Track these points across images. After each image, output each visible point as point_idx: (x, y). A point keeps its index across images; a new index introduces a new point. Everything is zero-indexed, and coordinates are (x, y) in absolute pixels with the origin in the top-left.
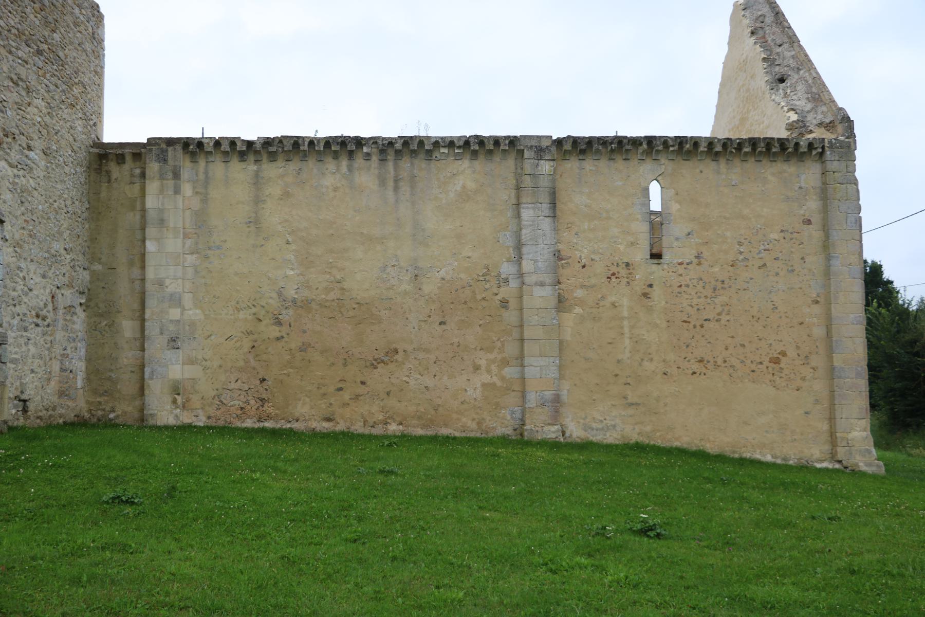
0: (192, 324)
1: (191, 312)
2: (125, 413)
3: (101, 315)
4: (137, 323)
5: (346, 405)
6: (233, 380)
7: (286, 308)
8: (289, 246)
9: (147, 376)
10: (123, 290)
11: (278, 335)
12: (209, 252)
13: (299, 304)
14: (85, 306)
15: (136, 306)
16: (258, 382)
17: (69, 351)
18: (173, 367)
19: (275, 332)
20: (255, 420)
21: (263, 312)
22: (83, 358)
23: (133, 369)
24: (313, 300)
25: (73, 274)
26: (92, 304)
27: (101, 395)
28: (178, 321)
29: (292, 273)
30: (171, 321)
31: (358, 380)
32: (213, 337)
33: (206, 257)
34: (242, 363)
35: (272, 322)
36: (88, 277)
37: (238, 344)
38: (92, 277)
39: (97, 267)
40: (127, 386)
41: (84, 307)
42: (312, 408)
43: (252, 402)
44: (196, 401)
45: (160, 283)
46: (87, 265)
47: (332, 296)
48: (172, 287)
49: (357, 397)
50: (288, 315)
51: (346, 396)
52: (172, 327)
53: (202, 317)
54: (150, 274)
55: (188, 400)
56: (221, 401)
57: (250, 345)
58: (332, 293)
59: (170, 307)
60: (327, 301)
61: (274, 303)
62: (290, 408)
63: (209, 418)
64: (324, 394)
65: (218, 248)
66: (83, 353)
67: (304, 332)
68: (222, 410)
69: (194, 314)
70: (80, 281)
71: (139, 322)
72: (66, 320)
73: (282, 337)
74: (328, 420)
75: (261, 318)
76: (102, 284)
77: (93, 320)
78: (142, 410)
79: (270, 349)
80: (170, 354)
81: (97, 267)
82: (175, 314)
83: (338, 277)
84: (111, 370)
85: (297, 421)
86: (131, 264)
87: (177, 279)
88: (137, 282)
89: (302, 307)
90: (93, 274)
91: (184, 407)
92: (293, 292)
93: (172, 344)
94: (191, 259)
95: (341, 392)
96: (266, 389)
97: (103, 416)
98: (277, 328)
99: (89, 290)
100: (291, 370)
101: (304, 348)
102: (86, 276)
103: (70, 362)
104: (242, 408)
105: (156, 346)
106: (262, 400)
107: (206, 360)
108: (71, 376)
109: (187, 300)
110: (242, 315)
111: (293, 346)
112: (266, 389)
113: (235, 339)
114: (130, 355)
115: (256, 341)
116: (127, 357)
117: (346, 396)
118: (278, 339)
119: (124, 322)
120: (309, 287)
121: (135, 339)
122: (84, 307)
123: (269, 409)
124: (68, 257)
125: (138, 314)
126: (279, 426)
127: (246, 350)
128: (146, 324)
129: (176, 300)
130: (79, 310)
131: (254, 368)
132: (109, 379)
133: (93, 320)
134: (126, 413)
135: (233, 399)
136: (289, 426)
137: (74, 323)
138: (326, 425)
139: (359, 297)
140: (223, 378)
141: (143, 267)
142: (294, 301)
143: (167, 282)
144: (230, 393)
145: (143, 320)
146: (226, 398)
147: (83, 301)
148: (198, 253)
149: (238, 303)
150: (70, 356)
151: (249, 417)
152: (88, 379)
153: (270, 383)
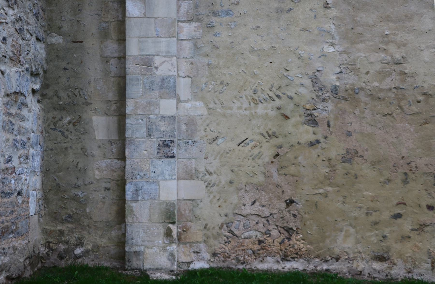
0: (191, 122)
1: (188, 105)
2: (97, 247)
3: (62, 108)
4: (113, 120)
5: (405, 238)
6: (248, 201)
7: (324, 100)
8: (327, 11)
9: (129, 196)
10: (94, 75)
11: (312, 138)
12: (214, 19)
13: (341, 94)
14: (41, 95)
15: (111, 95)
16: (284, 205)
17: (15, 162)
18: (161, 185)
19: (307, 134)
20: (278, 258)
21: (291, 106)
22: (38, 170)
23: (108, 185)
24: (362, 89)
25: (20, 41)
26: (50, 92)
27: (63, 222)
28: (173, 118)
29: (331, 49)
30: (163, 117)
31: (424, 204)
32: (220, 141)
33: (210, 27)
34: (260, 178)
35: (303, 119)
36: (43, 54)
37: (256, 151)
38: (48, 53)
39: (57, 40)
40: (100, 208)
41: (38, 96)
42: (358, 242)
43: (275, 233)
44: (196, 232)
45: (147, 63)
46: (41, 34)
47: (388, 83)
48: (164, 68)
49: (422, 227)
50: (326, 110)
51: (406, 225)
52: (163, 127)
53: (205, 112)
54: (133, 49)
55: (185, 230)
56: (231, 232)
57: (273, 152)
58: (388, 80)
59: (161, 97)
60: (381, 90)
61: (306, 93)
62: (328, 241)
63: (214, 255)
64: (376, 223)
65: (227, 13)
66: (37, 162)
67: (349, 134)
68: (233, 243)
69: (194, 108)
70: (31, 56)
71: (115, 118)
72: (10, 114)
73: (318, 142)
74: (381, 259)
75: (288, 113)
76: (64, 64)
77: (50, 115)
78: (122, 242)
79: (300, 159)
80: (162, 166)
81: (57, 40)
82: (168, 107)
83: (398, 56)
84: (78, 187)
85: (337, 259)
86: (104, 35)
87: (171, 57)
88: (113, 62)
89: (346, 99)
90: (51, 49)
91: (179, 239)
92: (334, 77)
93: (166, 150)
94: (188, 29)
95: (399, 221)
96: (295, 216)
97: (66, 251)
98: (310, 129)
99: (45, 72)
100: (330, 189)
101: (349, 157)
102: (40, 49)
103: (18, 180)
104: (260, 242)
105: (141, 152)
106: (289, 230)
107: (210, 174)
108: (20, 200)
109: (184, 87)
110: (261, 110)
111: (333, 154)
112: (295, 216)
113: (252, 144)
114: (104, 165)
115: (280, 147)
116: (100, 168)
117: (406, 225)
118: (311, 144)
119: (94, 118)
120: (356, 71)
121: (111, 142)
122: (38, 96)
123: (297, 242)
124: (11, 12)
125: (114, 107)
126: (311, 267)
127: (267, 160)
128: (128, 121)
129: (168, 88)
130: (31, 100)
131: (278, 186)
132: (75, 198)
133: (50, 115)
134: (98, 247)
135: (247, 228)
136: (325, 267)
137: (23, 119)
138: (377, 266)
139: (426, 85)
140: (234, 199)
141: (122, 40)
142: (335, 90)
143: (157, 61)
144: (244, 221)
145: (122, 116)
146: (238, 227)
147: (37, 87)
148: (198, 20)
149: (255, 92)
150: (18, 171)
151: (270, 254)
152: (45, 199)
153: (300, 206)
